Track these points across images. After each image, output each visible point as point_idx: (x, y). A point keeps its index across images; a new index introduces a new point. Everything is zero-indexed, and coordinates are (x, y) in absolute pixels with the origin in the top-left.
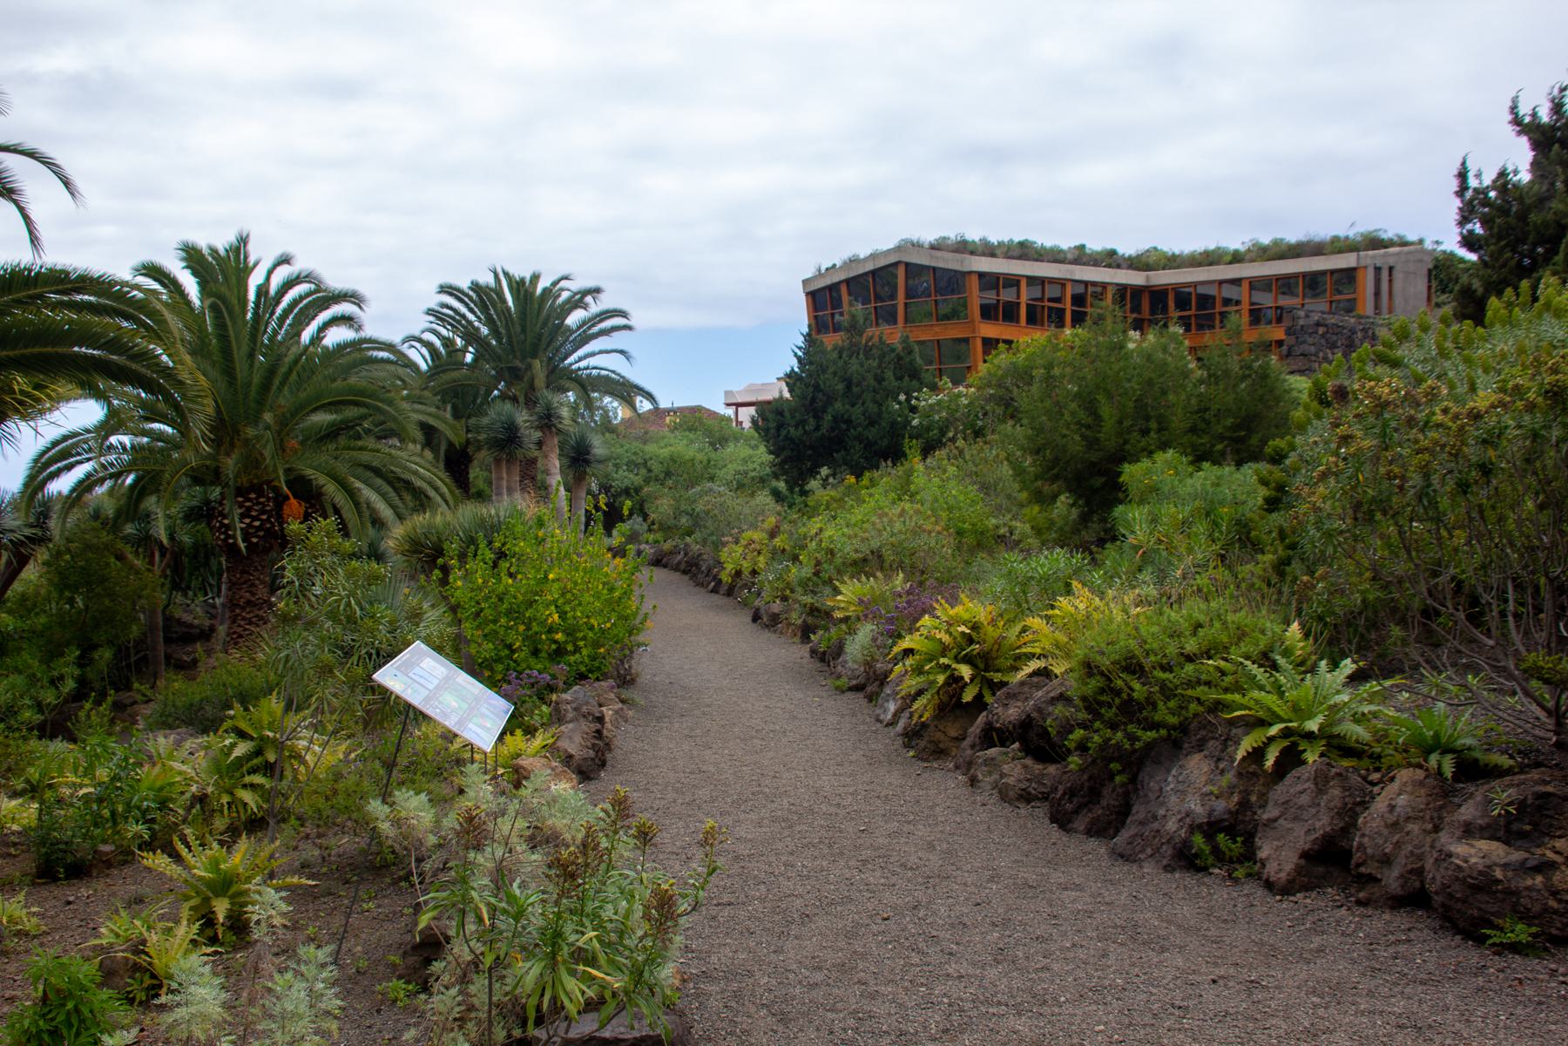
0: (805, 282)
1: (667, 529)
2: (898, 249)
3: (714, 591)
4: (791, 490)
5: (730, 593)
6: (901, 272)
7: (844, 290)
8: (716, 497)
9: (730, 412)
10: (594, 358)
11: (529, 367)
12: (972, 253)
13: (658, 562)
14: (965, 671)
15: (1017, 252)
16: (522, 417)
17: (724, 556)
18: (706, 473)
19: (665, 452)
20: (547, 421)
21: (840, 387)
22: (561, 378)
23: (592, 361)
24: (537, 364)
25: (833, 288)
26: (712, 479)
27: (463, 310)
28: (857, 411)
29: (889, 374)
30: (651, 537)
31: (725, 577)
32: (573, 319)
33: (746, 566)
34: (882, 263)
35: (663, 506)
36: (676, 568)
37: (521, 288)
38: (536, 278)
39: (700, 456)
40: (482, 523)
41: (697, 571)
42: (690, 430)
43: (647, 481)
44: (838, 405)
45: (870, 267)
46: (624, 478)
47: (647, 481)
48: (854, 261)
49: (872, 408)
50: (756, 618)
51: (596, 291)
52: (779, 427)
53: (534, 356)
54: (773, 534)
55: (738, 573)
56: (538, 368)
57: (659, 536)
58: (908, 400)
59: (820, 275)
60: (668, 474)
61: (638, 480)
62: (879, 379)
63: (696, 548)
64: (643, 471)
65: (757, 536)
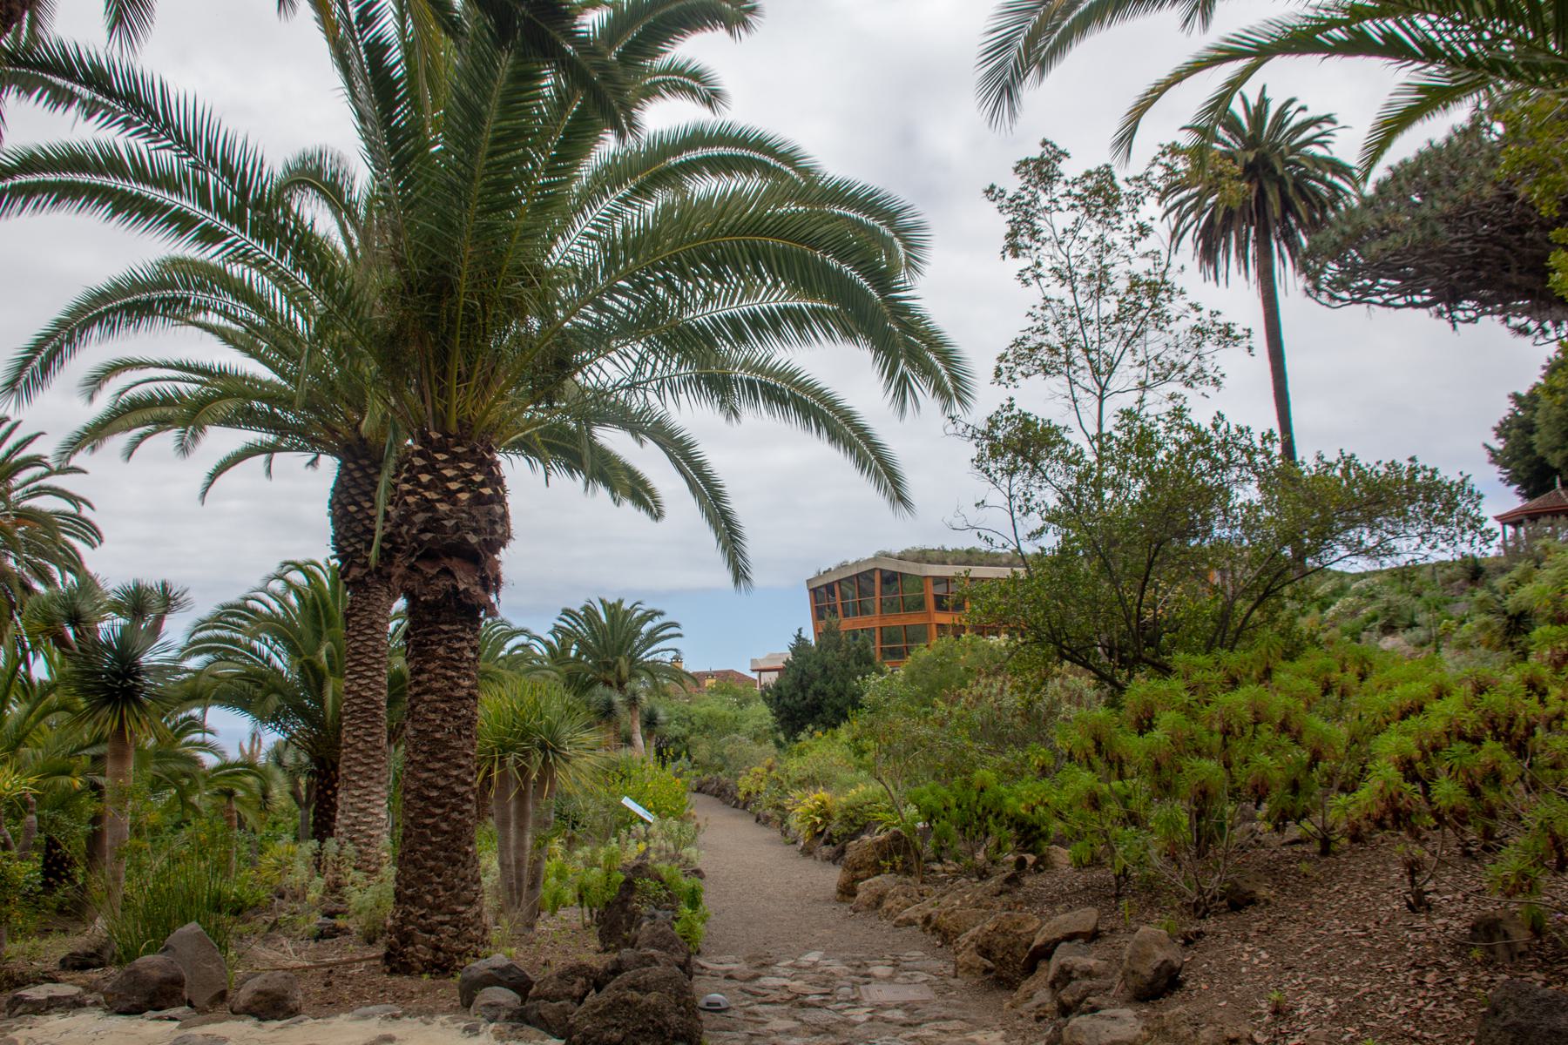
1: (706, 767)
2: (875, 559)
4: (787, 739)
5: (744, 807)
8: (741, 744)
9: (755, 676)
10: (660, 654)
12: (929, 562)
14: (818, 820)
15: (966, 557)
16: (617, 699)
17: (740, 782)
19: (704, 711)
20: (633, 702)
21: (819, 671)
22: (637, 668)
23: (659, 656)
24: (622, 660)
25: (829, 588)
26: (737, 730)
28: (829, 688)
29: (852, 662)
30: (694, 773)
31: (741, 796)
32: (645, 629)
33: (753, 788)
34: (864, 569)
35: (702, 750)
36: (711, 794)
37: (613, 610)
38: (621, 602)
39: (730, 714)
41: (723, 794)
42: (723, 693)
43: (691, 732)
44: (817, 683)
45: (855, 572)
46: (674, 730)
47: (691, 732)
48: (844, 566)
49: (839, 684)
50: (758, 820)
51: (661, 613)
52: (779, 698)
53: (620, 654)
54: (770, 769)
55: (749, 794)
57: (699, 772)
59: (819, 576)
60: (707, 726)
61: (685, 731)
62: (846, 666)
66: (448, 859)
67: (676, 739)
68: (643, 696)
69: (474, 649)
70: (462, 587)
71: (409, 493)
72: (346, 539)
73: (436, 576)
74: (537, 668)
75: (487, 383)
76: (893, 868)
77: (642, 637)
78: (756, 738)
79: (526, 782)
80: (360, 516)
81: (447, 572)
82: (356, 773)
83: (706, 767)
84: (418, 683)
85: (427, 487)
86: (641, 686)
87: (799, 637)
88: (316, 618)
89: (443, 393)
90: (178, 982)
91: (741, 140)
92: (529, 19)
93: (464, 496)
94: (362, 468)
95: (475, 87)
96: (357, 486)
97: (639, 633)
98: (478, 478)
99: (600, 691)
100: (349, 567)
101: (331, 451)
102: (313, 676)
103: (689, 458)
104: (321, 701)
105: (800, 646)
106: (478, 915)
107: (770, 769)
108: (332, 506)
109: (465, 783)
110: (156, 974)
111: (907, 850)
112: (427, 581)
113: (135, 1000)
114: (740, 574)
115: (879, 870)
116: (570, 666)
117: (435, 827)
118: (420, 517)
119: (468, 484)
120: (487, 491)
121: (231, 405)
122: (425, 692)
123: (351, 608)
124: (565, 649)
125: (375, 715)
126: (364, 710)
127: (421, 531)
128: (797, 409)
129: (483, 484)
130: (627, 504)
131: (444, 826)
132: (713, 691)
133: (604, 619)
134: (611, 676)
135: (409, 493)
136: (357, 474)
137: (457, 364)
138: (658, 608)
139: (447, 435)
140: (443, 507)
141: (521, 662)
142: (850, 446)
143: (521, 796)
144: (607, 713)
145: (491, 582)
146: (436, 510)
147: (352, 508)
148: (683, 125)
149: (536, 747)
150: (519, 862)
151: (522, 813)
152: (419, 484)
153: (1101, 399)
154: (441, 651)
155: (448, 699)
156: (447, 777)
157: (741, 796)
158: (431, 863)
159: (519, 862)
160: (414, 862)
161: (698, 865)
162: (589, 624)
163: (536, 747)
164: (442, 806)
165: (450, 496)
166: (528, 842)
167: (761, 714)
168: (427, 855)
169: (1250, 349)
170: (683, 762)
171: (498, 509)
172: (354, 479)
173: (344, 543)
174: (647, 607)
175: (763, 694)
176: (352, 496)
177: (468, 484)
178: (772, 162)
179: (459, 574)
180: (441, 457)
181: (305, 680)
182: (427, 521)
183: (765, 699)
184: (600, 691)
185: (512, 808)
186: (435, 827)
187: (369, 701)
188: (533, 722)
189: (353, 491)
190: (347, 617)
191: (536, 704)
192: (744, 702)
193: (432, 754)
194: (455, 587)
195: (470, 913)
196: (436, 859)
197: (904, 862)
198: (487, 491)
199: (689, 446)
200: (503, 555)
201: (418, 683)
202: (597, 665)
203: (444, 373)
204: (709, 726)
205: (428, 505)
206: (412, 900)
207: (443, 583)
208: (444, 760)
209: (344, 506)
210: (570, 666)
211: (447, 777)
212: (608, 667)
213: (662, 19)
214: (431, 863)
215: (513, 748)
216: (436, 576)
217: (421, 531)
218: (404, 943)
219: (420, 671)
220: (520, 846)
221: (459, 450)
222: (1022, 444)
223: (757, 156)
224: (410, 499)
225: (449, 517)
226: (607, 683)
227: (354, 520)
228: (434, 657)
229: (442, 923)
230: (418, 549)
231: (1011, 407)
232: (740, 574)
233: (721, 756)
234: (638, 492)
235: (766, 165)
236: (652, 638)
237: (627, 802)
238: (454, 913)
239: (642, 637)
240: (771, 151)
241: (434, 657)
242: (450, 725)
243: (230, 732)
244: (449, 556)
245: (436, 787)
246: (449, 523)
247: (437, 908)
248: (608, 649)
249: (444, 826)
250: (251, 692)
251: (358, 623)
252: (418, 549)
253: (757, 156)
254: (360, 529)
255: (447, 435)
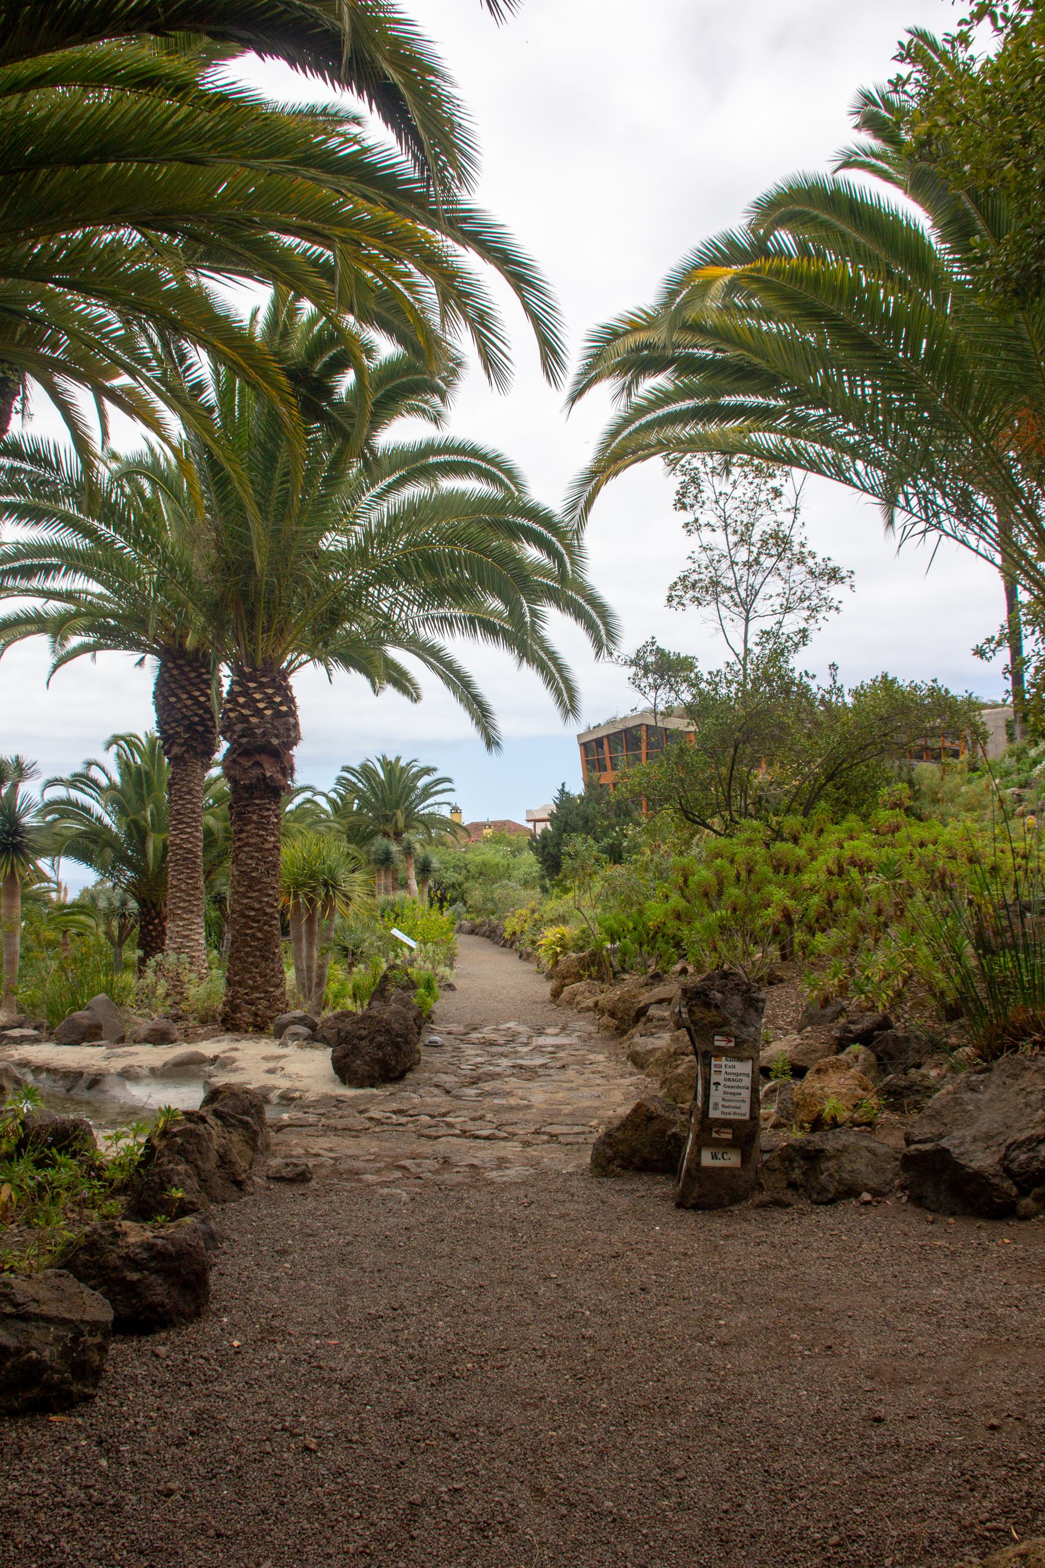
0: (579, 736)
1: (478, 911)
3: (503, 946)
6: (644, 728)
7: (605, 741)
9: (530, 826)
10: (438, 806)
11: (395, 814)
13: (472, 932)
14: (559, 949)
16: (395, 848)
17: (506, 923)
18: (506, 873)
19: (479, 859)
20: (408, 851)
22: (412, 819)
23: (434, 809)
24: (399, 813)
25: (599, 742)
26: (509, 878)
27: (354, 779)
30: (469, 917)
31: (506, 935)
32: (421, 783)
34: (631, 724)
35: (476, 895)
38: (398, 759)
40: (388, 903)
41: (492, 935)
42: (497, 843)
43: (467, 879)
45: (621, 727)
46: (451, 877)
47: (467, 879)
51: (435, 769)
52: (544, 847)
53: (397, 808)
54: (533, 912)
55: (514, 933)
56: (400, 815)
57: (473, 916)
58: (622, 830)
59: (589, 731)
60: (481, 874)
61: (460, 878)
63: (496, 922)
64: (464, 872)
65: (524, 912)
66: (263, 957)
67: (453, 886)
68: (418, 846)
69: (277, 816)
70: (268, 774)
71: (231, 710)
72: (168, 723)
73: (250, 767)
74: (323, 821)
75: (282, 631)
76: (590, 976)
77: (418, 792)
78: (525, 884)
79: (314, 909)
80: (179, 706)
81: (258, 764)
82: (180, 908)
83: (478, 911)
84: (239, 839)
85: (243, 706)
86: (416, 837)
87: (562, 792)
88: (139, 784)
89: (252, 640)
90: (99, 1027)
91: (460, 450)
92: (306, 397)
93: (268, 712)
94: (179, 667)
95: (272, 439)
96: (176, 681)
97: (415, 788)
98: (278, 699)
99: (380, 842)
100: (171, 746)
101: (153, 652)
102: (137, 832)
103: (440, 660)
104: (144, 854)
105: (564, 799)
106: (283, 994)
107: (533, 912)
108: (155, 697)
109: (272, 906)
110: (86, 1022)
111: (600, 964)
112: (245, 770)
113: (74, 1037)
114: (491, 742)
115: (579, 978)
116: (352, 819)
117: (253, 935)
118: (239, 727)
119: (271, 704)
120: (284, 708)
121: (82, 622)
122: (244, 846)
123: (173, 778)
124: (347, 804)
125: (194, 862)
126: (185, 859)
127: (240, 737)
128: (504, 638)
129: (281, 704)
130: (390, 690)
131: (259, 935)
132: (487, 841)
133: (382, 776)
134: (389, 828)
135: (231, 710)
136: (175, 672)
137: (261, 620)
138: (432, 765)
139: (255, 669)
140: (254, 720)
141: (308, 812)
142: (542, 667)
143: (311, 920)
144: (385, 860)
145: (288, 770)
146: (249, 722)
147: (173, 699)
148: (418, 440)
149: (320, 887)
150: (309, 968)
151: (311, 933)
152: (238, 704)
153: (747, 620)
154: (255, 817)
155: (261, 850)
156: (260, 902)
157: (506, 935)
158: (251, 959)
159: (309, 968)
160: (239, 959)
161: (451, 980)
162: (368, 780)
163: (320, 887)
164: (258, 922)
165: (259, 713)
166: (316, 954)
167: (529, 862)
168: (248, 954)
169: (852, 586)
170: (459, 906)
171: (292, 720)
172: (172, 676)
173: (166, 727)
174: (422, 764)
175: (530, 844)
176: (172, 690)
177: (271, 704)
178: (484, 465)
179: (266, 766)
180: (252, 685)
181: (129, 835)
182: (244, 730)
183: (531, 848)
184: (380, 842)
185: (304, 929)
186: (253, 935)
187: (190, 851)
188: (318, 866)
189: (173, 686)
190: (170, 785)
191: (320, 852)
192: (516, 852)
193: (250, 887)
194: (264, 775)
195: (278, 992)
196: (254, 956)
197: (599, 971)
198: (284, 708)
199: (440, 650)
200: (295, 751)
201: (239, 839)
202: (376, 817)
203: (252, 627)
204: (486, 873)
205: (244, 719)
206: (239, 983)
207: (255, 772)
208: (258, 891)
209: (165, 698)
210: (352, 819)
211: (260, 902)
212: (387, 819)
213: (397, 387)
214: (251, 959)
215: (304, 885)
216: (250, 767)
217: (240, 737)
218: (234, 1012)
219: (241, 831)
220: (310, 957)
221: (264, 680)
222: (664, 667)
223: (472, 461)
224: (232, 715)
225: (259, 728)
226: (386, 834)
227: (174, 708)
228: (250, 822)
229: (259, 998)
230: (220, 732)
231: (653, 643)
232: (491, 742)
233: (492, 900)
234: (402, 681)
235: (480, 467)
236: (427, 793)
237: (395, 932)
238: (266, 992)
239: (418, 792)
240: (483, 457)
241: (250, 822)
242: (262, 868)
243: (73, 878)
244: (259, 753)
245: (253, 909)
246: (258, 731)
247: (255, 988)
248: (386, 802)
249: (259, 935)
250: (88, 845)
251: (179, 790)
252: (220, 732)
253: (472, 461)
254: (179, 716)
255: (255, 669)
